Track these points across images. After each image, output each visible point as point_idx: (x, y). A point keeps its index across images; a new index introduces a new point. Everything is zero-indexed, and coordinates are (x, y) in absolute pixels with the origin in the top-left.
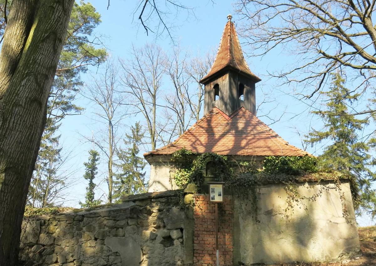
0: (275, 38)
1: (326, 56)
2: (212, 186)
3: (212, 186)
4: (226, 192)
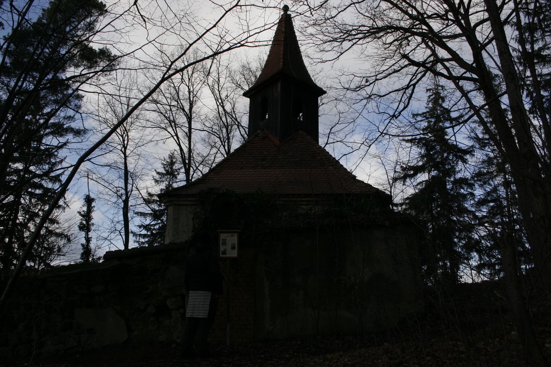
0: (350, 38)
1: (413, 63)
2: (222, 236)
3: (222, 236)
4: (242, 245)
